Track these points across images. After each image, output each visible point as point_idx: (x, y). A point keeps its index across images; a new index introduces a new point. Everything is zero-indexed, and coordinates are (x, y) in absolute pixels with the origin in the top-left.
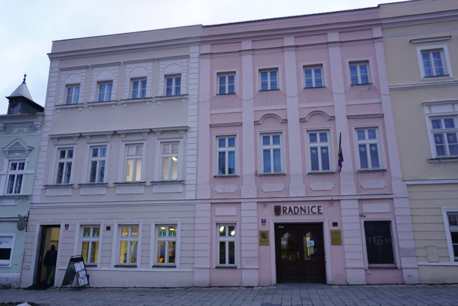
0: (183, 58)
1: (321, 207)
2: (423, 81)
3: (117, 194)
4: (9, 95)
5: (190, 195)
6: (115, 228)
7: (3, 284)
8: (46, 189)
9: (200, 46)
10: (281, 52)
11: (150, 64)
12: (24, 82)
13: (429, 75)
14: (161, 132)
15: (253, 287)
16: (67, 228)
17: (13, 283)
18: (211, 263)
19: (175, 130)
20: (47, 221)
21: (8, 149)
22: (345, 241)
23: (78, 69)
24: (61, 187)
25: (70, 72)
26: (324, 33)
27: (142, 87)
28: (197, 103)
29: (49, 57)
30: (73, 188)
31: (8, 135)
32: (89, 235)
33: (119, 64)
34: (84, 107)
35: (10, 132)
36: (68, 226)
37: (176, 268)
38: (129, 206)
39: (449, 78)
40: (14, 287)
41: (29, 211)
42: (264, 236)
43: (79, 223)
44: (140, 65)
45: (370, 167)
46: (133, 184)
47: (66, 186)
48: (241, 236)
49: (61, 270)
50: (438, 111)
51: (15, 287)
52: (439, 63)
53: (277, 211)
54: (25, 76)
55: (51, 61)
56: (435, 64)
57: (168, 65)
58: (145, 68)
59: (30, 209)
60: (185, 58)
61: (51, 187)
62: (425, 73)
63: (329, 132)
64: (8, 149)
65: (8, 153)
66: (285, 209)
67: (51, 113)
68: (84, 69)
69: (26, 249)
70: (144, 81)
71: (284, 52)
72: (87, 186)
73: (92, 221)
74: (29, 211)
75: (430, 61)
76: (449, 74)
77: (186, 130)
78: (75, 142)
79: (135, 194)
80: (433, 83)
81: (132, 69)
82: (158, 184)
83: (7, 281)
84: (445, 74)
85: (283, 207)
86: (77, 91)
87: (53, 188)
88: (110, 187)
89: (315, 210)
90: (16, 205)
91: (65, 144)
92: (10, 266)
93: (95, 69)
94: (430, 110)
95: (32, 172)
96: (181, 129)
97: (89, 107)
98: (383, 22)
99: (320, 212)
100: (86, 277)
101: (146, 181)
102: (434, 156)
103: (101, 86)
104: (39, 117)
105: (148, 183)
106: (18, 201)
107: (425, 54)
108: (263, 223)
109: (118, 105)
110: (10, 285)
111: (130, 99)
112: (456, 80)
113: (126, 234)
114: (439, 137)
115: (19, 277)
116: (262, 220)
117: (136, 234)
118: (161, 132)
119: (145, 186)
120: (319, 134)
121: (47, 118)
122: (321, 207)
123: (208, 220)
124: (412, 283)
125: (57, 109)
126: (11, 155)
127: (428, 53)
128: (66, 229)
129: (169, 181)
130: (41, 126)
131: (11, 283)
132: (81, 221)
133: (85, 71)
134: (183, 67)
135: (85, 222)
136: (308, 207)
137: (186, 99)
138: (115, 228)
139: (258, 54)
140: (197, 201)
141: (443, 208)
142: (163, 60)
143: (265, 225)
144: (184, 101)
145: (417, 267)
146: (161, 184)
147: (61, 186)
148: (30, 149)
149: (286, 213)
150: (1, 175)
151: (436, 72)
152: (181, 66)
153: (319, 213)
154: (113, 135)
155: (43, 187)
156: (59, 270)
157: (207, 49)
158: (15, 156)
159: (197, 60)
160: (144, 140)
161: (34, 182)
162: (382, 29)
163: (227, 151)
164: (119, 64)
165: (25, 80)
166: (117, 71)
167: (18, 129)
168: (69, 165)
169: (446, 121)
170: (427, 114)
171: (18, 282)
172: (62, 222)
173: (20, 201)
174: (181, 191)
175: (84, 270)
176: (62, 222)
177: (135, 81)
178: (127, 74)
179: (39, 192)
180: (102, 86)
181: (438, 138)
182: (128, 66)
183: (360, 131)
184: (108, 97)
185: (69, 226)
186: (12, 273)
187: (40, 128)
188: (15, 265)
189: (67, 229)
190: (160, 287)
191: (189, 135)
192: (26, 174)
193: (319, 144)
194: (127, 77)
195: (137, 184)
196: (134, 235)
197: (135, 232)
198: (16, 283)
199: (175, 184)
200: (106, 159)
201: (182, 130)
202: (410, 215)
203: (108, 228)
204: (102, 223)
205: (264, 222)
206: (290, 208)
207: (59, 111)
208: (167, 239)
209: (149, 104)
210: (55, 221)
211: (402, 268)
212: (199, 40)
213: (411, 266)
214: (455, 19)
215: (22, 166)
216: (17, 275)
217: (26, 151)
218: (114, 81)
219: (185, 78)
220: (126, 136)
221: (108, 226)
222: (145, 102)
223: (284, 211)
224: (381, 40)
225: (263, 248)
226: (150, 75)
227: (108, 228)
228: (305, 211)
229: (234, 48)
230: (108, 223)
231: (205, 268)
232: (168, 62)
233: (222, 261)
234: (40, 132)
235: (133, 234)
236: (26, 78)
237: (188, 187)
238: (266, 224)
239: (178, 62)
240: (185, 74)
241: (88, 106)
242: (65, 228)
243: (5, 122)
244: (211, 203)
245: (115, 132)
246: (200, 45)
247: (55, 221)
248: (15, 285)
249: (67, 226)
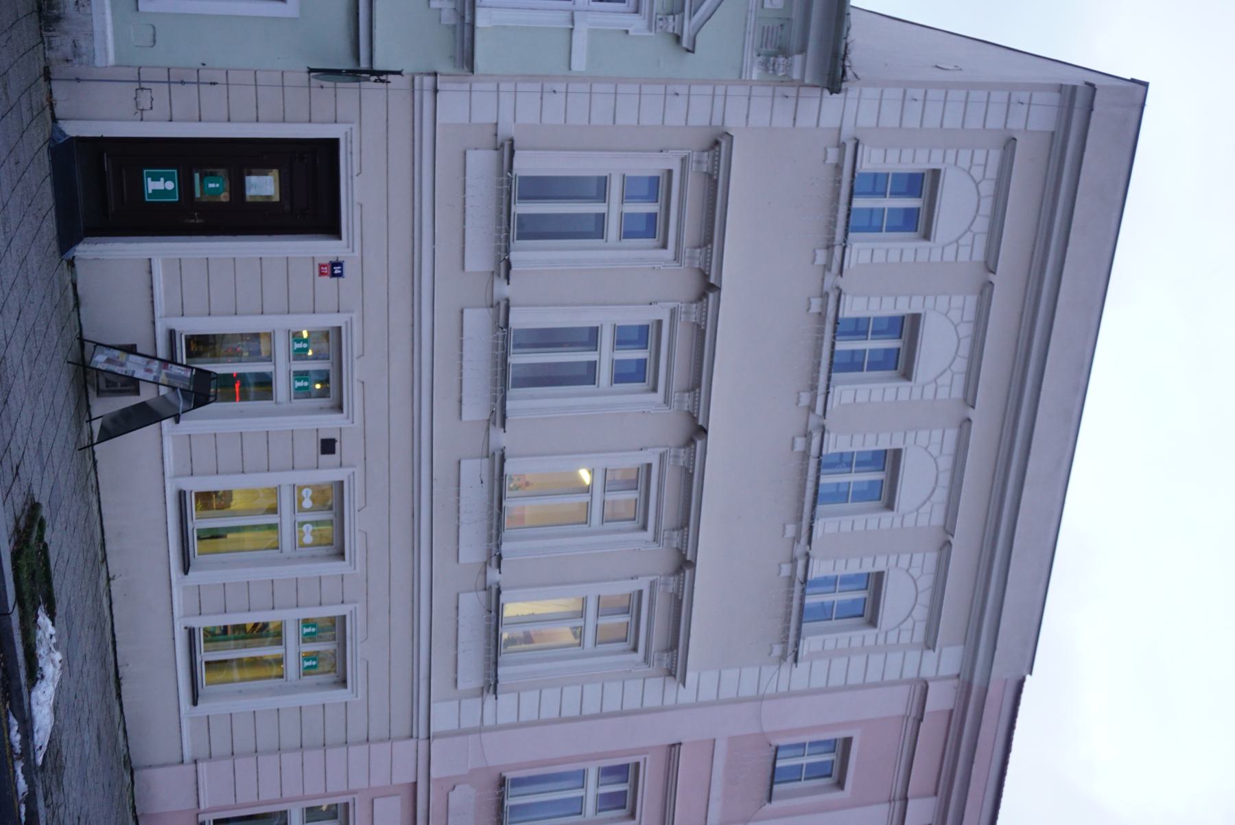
0: (928, 629)
5: (443, 718)
6: (328, 474)
9: (958, 676)
10: (891, 792)
17: (66, 33)
19: (676, 642)
20: (356, 171)
23: (931, 613)
24: (500, 231)
25: (987, 188)
28: (761, 692)
32: (310, 638)
33: (969, 400)
34: (827, 273)
36: (333, 275)
37: (192, 707)
38: (415, 515)
40: (50, 43)
41: (399, 73)
43: (346, 323)
44: (986, 206)
45: (517, 359)
46: (494, 532)
47: (503, 255)
51: (50, 48)
56: (838, 484)
57: (919, 596)
61: (505, 186)
63: (656, 248)
67: (830, 118)
69: (228, 89)
72: (500, 352)
74: (399, 73)
75: (867, 339)
77: (675, 671)
78: (675, 396)
82: (489, 619)
88: (488, 429)
95: (580, 63)
97: (824, 296)
108: (329, 267)
110: (58, 19)
113: (308, 539)
117: (307, 504)
119: (486, 564)
120: (654, 211)
123: (358, 782)
125: (841, 146)
128: (321, 266)
129: (503, 505)
131: (65, 25)
135: (352, 345)
137: (783, 658)
139: (900, 739)
140: (426, 742)
141: (358, 609)
144: (777, 650)
146: (489, 627)
147: (503, 235)
154: (705, 276)
156: (150, 259)
157: (940, 700)
159: (910, 673)
160: (656, 533)
161: (530, 78)
163: (606, 209)
164: (969, 400)
168: (587, 375)
169: (642, 363)
172: (351, 246)
173: (448, 18)
176: (351, 246)
177: (890, 461)
179: (484, 115)
183: (655, 187)
185: (335, 279)
186: (113, 14)
189: (322, 274)
190: (119, 663)
191: (654, 684)
192: (572, 29)
193: (606, 356)
195: (500, 338)
196: (301, 500)
197: (313, 499)
198: (67, 49)
199: (486, 678)
200: (607, 319)
203: (328, 446)
204: (348, 418)
208: (282, 370)
212: (976, 681)
216: (105, 50)
218: (904, 386)
221: (337, 445)
222: (785, 641)
226: (897, 524)
227: (328, 446)
230: (348, 447)
231: (198, 795)
232: (926, 582)
234: (756, 74)
235: (308, 493)
237: (473, 704)
238: (327, 278)
239: (921, 613)
240: (870, 641)
241: (827, 294)
242: (327, 262)
245: (703, 431)
246: (961, 677)
247: (357, 387)
248: (62, 44)
249: (334, 269)
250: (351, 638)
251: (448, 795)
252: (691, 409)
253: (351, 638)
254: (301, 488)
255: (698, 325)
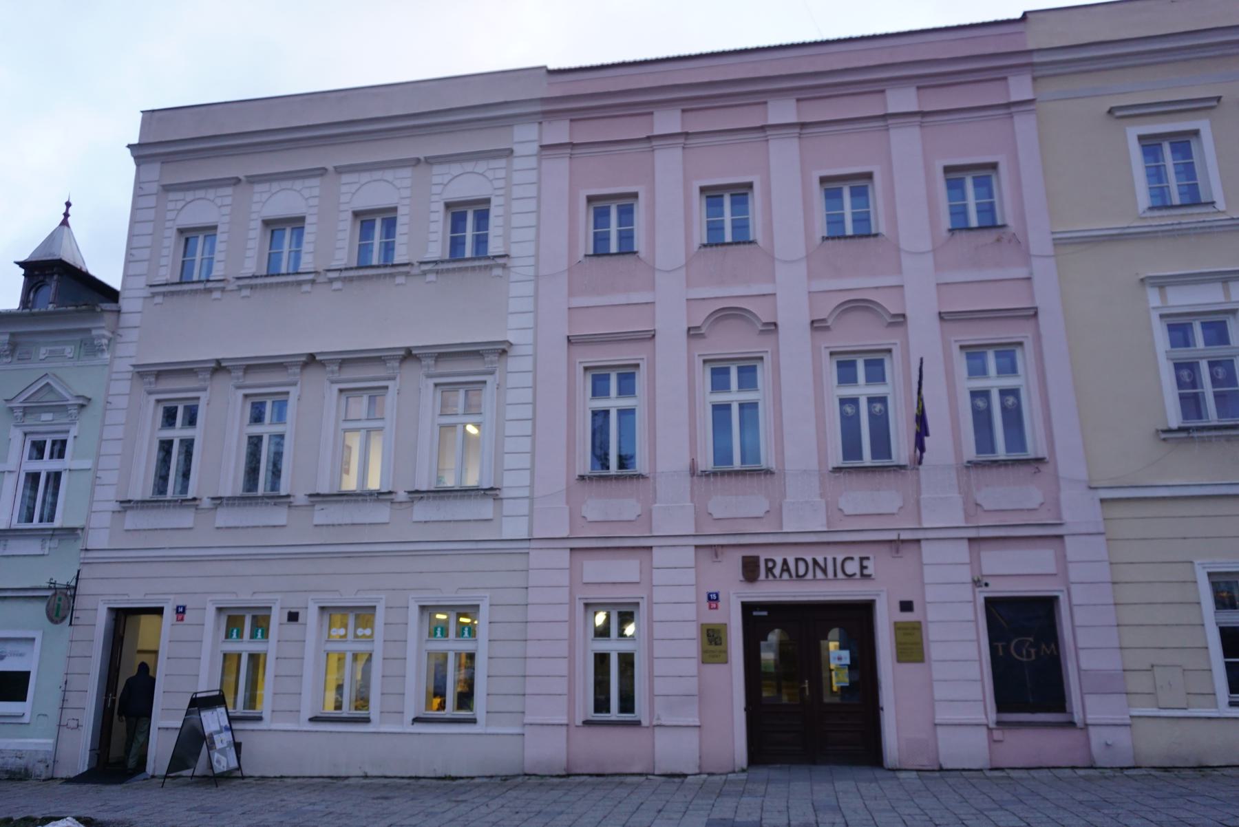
0: (494, 158)
1: (868, 558)
2: (1145, 218)
3: (316, 526)
4: (24, 257)
5: (515, 528)
6: (311, 617)
7: (8, 769)
8: (125, 510)
9: (540, 123)
10: (760, 141)
11: (406, 172)
12: (65, 223)
13: (1161, 203)
14: (437, 357)
15: (685, 776)
16: (180, 617)
17: (34, 765)
18: (571, 712)
19: (473, 352)
20: (126, 597)
21: (21, 402)
22: (935, 651)
23: (211, 187)
24: (164, 506)
25: (190, 196)
26: (877, 88)
27: (384, 235)
28: (532, 278)
29: (133, 154)
30: (197, 509)
31: (23, 366)
32: (240, 635)
33: (322, 172)
34: (226, 289)
35: (26, 356)
36: (184, 612)
37: (477, 724)
38: (349, 556)
39: (1214, 210)
41: (79, 571)
42: (713, 637)
43: (213, 604)
44: (377, 175)
45: (1001, 453)
46: (360, 498)
47: (178, 504)
48: (651, 639)
49: (165, 730)
50: (1184, 299)
51: (40, 776)
52: (1187, 170)
53: (750, 569)
54: (68, 205)
55: (138, 165)
56: (1177, 173)
57: (455, 175)
58: (391, 183)
59: (82, 565)
60: (500, 157)
61: (139, 505)
62: (1149, 197)
63: (891, 357)
64: (21, 402)
65: (21, 414)
66: (770, 565)
67: (137, 305)
68: (228, 185)
69: (71, 674)
70: (389, 218)
71: (767, 140)
72: (236, 502)
73: (249, 597)
74: (79, 571)
75: (1164, 166)
76: (1215, 200)
77: (503, 350)
78: (202, 384)
79: (365, 524)
80: (1172, 224)
81: (357, 186)
82: (429, 498)
83: (18, 759)
84: (1203, 201)
85: (767, 561)
86: (207, 247)
87: (142, 508)
88: (296, 506)
89: (852, 567)
90: (43, 555)
91: (176, 389)
92: (26, 719)
93: (258, 188)
94: (1163, 297)
95: (87, 464)
96: (489, 350)
97: (240, 288)
98: (1036, 59)
99: (866, 572)
100: (233, 748)
101: (395, 490)
102: (1175, 420)
103: (273, 231)
104: (106, 316)
105: (402, 496)
106: (48, 544)
107: (1150, 145)
108: (712, 602)
109: (320, 283)
110: (26, 769)
111: (351, 269)
112: (1235, 217)
113: (342, 632)
114: (1189, 371)
115: (50, 748)
116: (709, 595)
117: (368, 632)
118: (437, 357)
119: (392, 502)
120: (863, 362)
121: (126, 320)
122: (868, 558)
123: (563, 595)
124: (1114, 766)
125: (154, 295)
126: (29, 420)
127: (1157, 144)
128: (177, 620)
130: (110, 340)
131: (30, 766)
132: (219, 597)
133: (229, 191)
134: (494, 182)
135: (230, 600)
136: (834, 559)
137: (504, 266)
138: (311, 617)
139: (699, 147)
140: (532, 542)
141: (1199, 562)
142: (441, 163)
143: (717, 608)
144: (497, 272)
145: (1129, 721)
146: (434, 498)
147: (166, 504)
148: (81, 402)
149: (774, 576)
150: (4, 472)
151: (1180, 194)
152: (491, 178)
153: (862, 575)
154: (305, 365)
155: (117, 507)
156: (159, 728)
157: (559, 132)
158: (40, 423)
159: (533, 162)
160: (389, 379)
161: (93, 492)
162: (1034, 79)
163: (613, 409)
164: (322, 172)
165: (66, 215)
166: (316, 192)
167: (49, 348)
168: (188, 445)
169: (1205, 326)
170: (1154, 308)
171: (48, 762)
172: (167, 601)
173: (54, 543)
174: (490, 516)
175: (226, 729)
176: (167, 601)
177: (364, 219)
178: (343, 199)
179: (106, 519)
180: (276, 232)
181: (1185, 373)
182: (346, 178)
183: (974, 353)
184: (292, 263)
185: (187, 612)
186: (31, 738)
187: (108, 345)
188: (41, 717)
189: (182, 620)
191: (512, 364)
192: (70, 470)
193: (862, 390)
194: (343, 207)
196: (364, 636)
197: (365, 628)
198: (42, 766)
199: (472, 498)
200: (287, 429)
201: (493, 352)
202: (1110, 580)
203: (293, 617)
204: (275, 603)
205: (713, 599)
206: (785, 562)
207: (159, 299)
208: (453, 646)
209: (404, 282)
210: (148, 597)
211: (1087, 725)
212: (539, 108)
213: (1112, 719)
214: (1231, 51)
215: (60, 449)
216: (45, 744)
217: (69, 408)
218: (309, 220)
219: (500, 211)
220: (340, 367)
221: (293, 610)
223: (769, 570)
224: (1032, 107)
225: (711, 669)
226: (407, 201)
227: (293, 617)
228: (824, 571)
229: (633, 129)
230: (293, 604)
231: (553, 725)
232: (456, 169)
233: (601, 704)
234: (107, 356)
235: (360, 632)
236: (71, 211)
237: (508, 507)
238: (720, 604)
239: (481, 166)
240: (501, 201)
241: (239, 286)
242: (175, 616)
243: (13, 330)
244: (572, 549)
245: (312, 357)
246: (540, 121)
247: (148, 597)
248: (40, 769)
249: (181, 611)
250: (794, 596)
251: (986, 511)
252: (299, 367)
253: (794, 596)
254: (356, 636)
255: (341, 363)
